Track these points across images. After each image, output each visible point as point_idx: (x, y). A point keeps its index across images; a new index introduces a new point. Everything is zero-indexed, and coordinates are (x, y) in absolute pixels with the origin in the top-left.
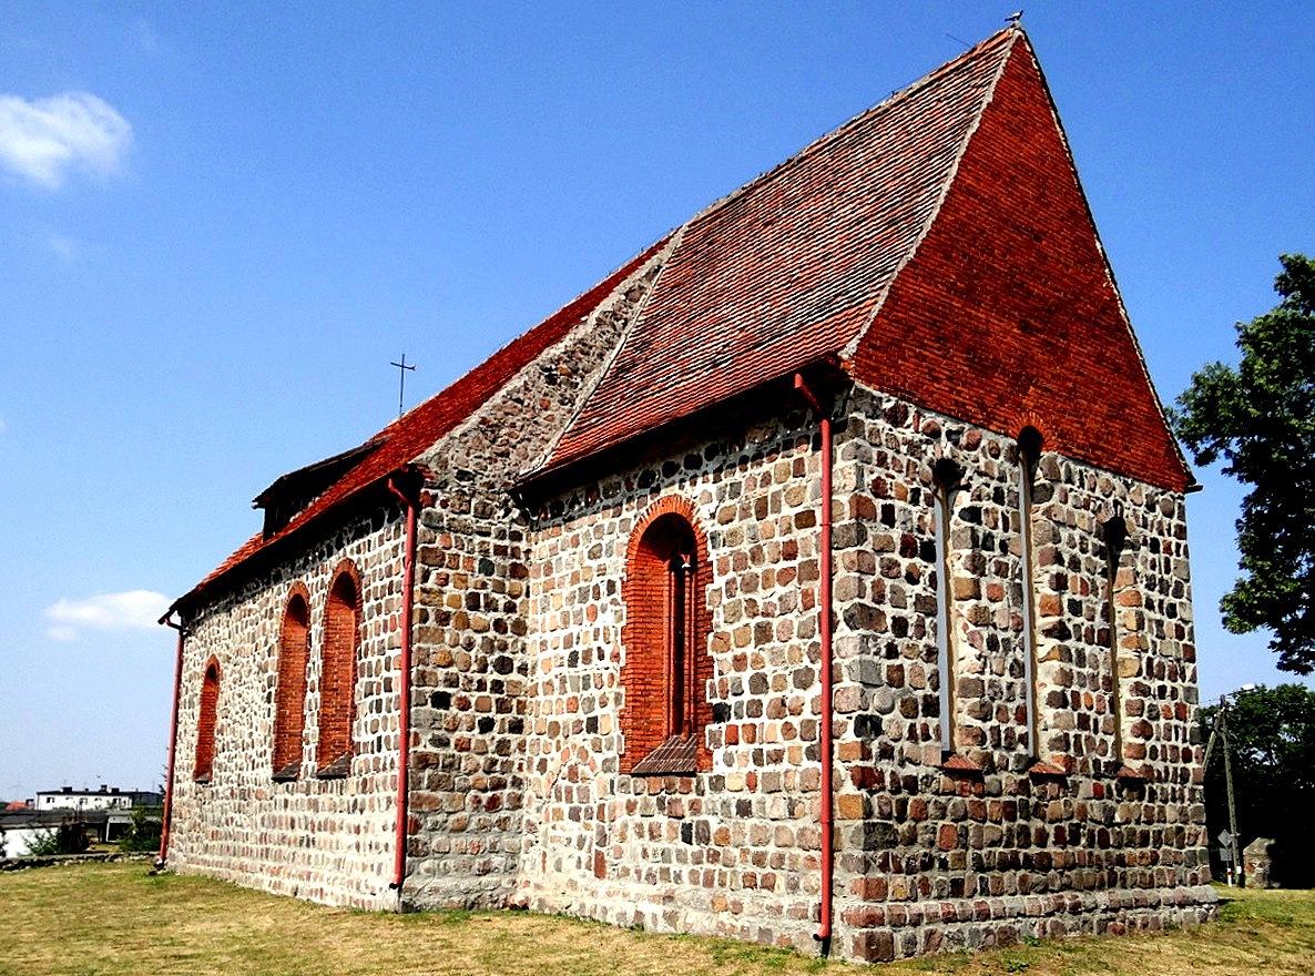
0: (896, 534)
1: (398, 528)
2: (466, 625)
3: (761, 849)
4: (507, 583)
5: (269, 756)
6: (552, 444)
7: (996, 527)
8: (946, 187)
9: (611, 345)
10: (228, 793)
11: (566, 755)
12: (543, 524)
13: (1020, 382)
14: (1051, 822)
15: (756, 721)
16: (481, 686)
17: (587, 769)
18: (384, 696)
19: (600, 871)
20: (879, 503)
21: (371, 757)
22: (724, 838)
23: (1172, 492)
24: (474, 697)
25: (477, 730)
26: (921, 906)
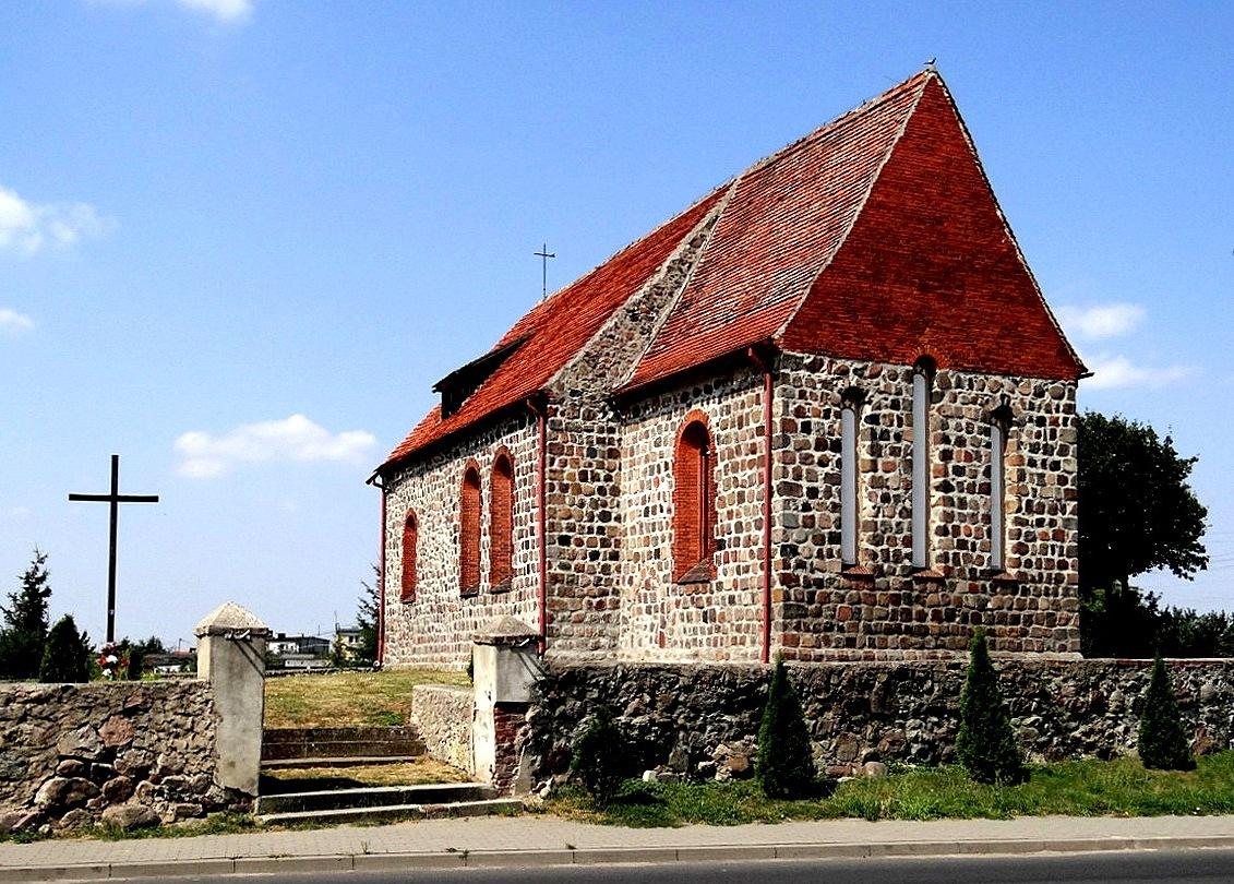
0: (812, 438)
1: (534, 429)
2: (579, 491)
3: (739, 622)
4: (606, 462)
5: (457, 581)
6: (635, 364)
7: (892, 425)
8: (860, 208)
9: (679, 284)
10: (429, 609)
11: (643, 575)
12: (629, 422)
13: (916, 329)
14: (930, 607)
15: (737, 549)
16: (590, 530)
17: (655, 581)
18: (530, 538)
19: (662, 645)
20: (799, 421)
21: (523, 577)
22: (723, 618)
23: (1062, 381)
25: (588, 559)
26: (823, 651)
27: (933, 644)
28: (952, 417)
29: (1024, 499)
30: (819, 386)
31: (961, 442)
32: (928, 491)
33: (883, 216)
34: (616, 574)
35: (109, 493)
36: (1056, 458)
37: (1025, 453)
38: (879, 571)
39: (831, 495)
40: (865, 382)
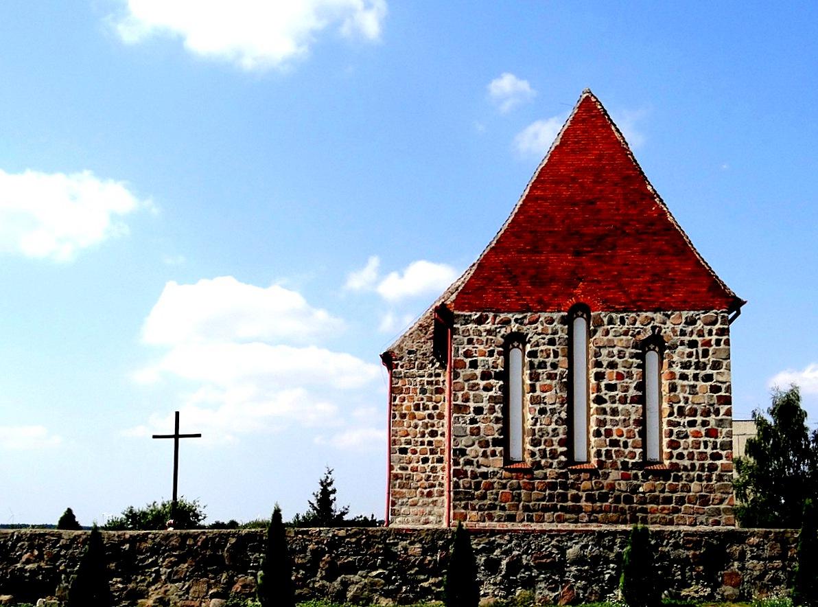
0: (478, 372)
2: (414, 417)
4: (433, 397)
14: (584, 491)
16: (422, 443)
20: (468, 360)
23: (715, 311)
24: (419, 448)
25: (421, 463)
27: (587, 519)
28: (605, 347)
29: (676, 406)
30: (484, 334)
31: (612, 365)
32: (588, 405)
33: (540, 205)
34: (441, 472)
35: (173, 433)
36: (708, 371)
37: (677, 370)
38: (537, 465)
39: (495, 412)
40: (525, 328)
